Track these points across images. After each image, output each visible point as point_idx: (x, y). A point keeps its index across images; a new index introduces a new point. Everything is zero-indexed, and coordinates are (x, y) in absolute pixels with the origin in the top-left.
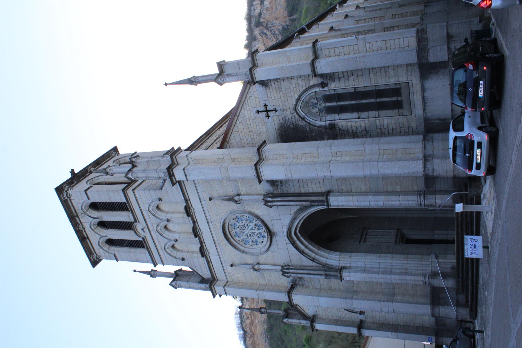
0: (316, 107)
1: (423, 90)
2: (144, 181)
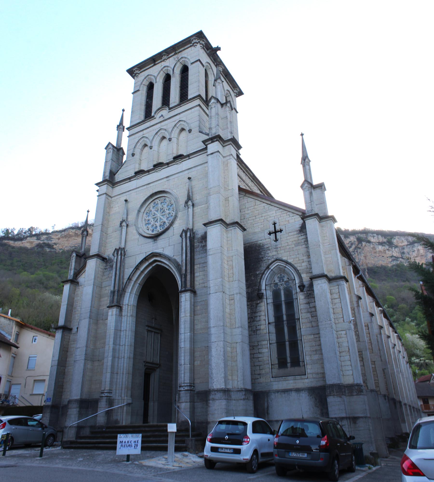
0: (280, 281)
1: (298, 390)
2: (208, 115)
